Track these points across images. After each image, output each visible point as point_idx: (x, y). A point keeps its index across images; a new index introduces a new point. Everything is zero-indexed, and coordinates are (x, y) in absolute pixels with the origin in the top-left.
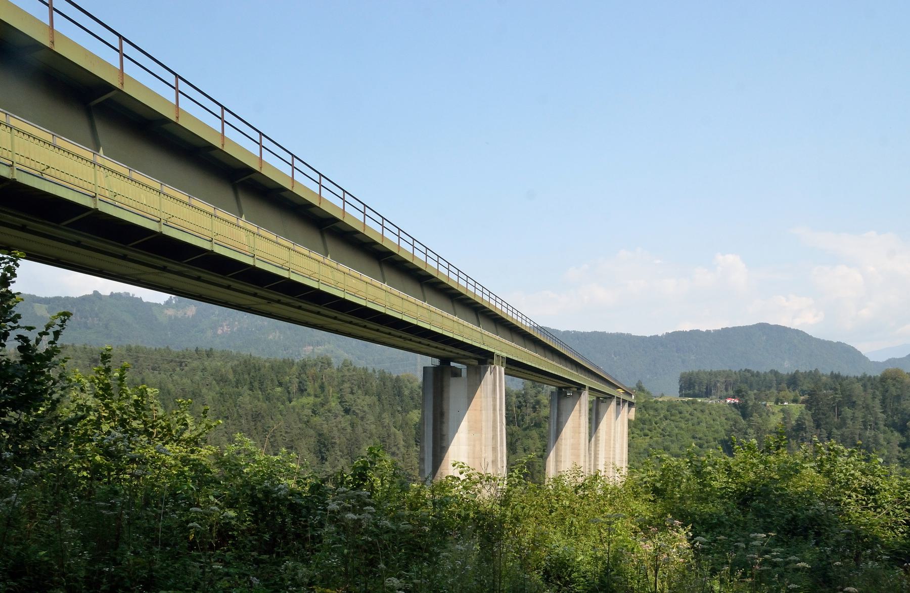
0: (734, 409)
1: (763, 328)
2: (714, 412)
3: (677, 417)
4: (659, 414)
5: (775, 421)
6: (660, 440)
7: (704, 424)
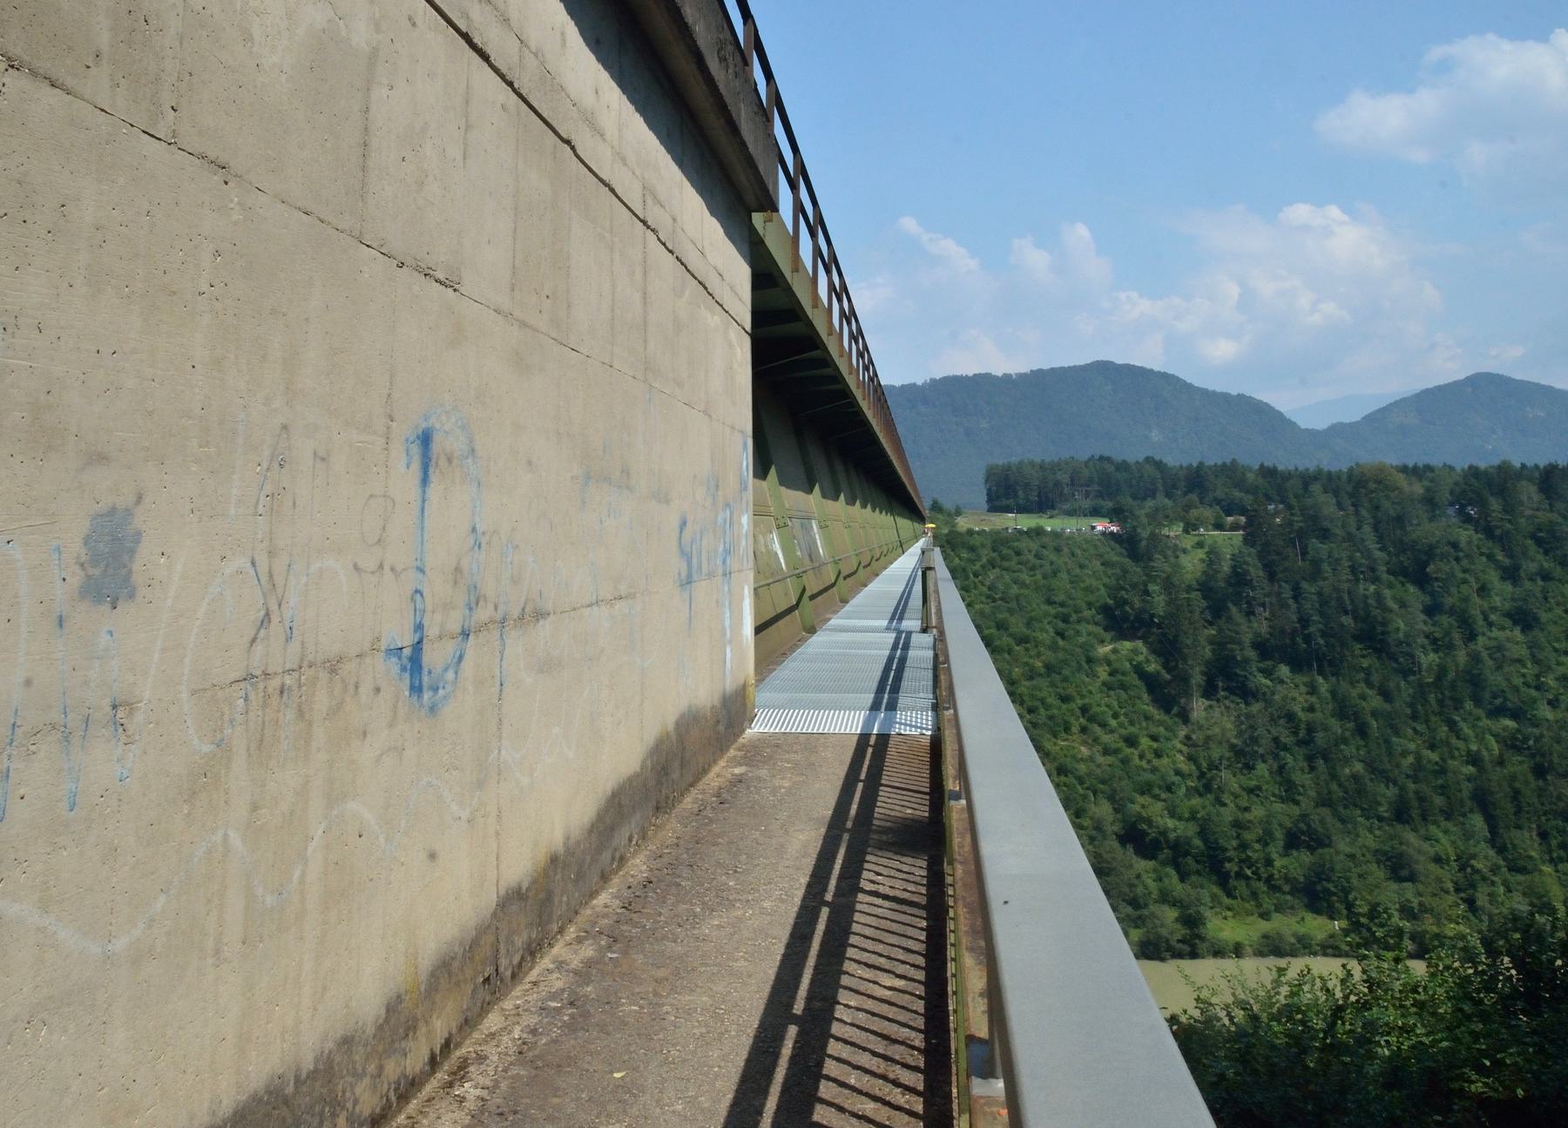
3: (1013, 564)
4: (979, 558)
5: (1192, 564)
6: (987, 609)
7: (1064, 576)
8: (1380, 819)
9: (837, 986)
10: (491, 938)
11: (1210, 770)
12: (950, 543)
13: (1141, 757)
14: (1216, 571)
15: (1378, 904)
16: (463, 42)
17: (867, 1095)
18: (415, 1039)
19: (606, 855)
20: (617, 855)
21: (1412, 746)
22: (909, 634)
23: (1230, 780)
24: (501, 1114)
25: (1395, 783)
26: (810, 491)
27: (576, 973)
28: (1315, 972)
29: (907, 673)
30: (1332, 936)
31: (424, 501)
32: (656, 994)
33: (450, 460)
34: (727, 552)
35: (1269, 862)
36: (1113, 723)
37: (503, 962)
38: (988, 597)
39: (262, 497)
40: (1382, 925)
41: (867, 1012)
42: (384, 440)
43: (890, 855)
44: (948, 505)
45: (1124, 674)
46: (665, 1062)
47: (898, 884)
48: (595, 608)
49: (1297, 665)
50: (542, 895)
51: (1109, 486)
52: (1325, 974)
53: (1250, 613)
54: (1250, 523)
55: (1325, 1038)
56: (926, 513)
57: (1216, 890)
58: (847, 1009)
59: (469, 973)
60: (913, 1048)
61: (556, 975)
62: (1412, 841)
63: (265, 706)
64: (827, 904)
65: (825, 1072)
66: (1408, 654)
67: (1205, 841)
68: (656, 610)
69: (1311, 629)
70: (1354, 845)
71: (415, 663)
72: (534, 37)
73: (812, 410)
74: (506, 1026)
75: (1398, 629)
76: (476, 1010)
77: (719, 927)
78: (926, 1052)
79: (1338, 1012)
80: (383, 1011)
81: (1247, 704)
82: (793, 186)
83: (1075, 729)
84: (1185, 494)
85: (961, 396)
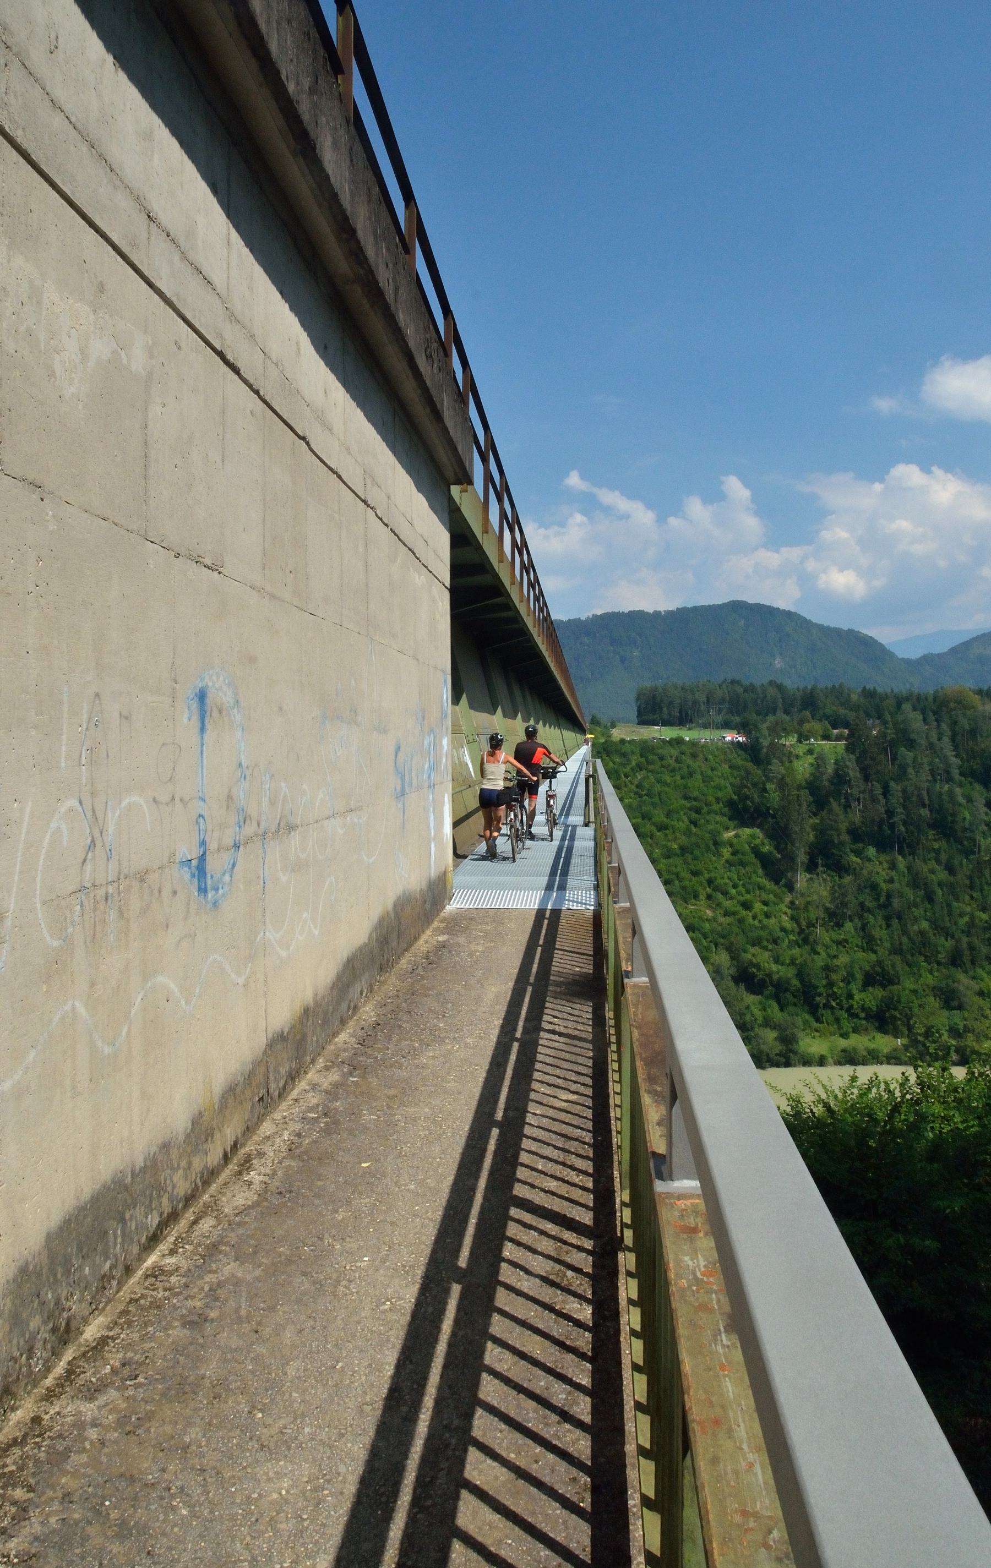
0: (740, 752)
1: (737, 606)
2: (711, 757)
3: (656, 767)
4: (629, 762)
5: (803, 768)
8: (939, 963)
9: (527, 1099)
10: (262, 1069)
11: (808, 927)
12: (602, 750)
13: (754, 918)
14: (822, 774)
15: (933, 1027)
16: (217, 359)
17: (552, 1176)
18: (213, 1142)
19: (344, 1006)
20: (352, 1005)
21: (968, 909)
22: (575, 827)
23: (822, 934)
24: (280, 1193)
25: (953, 937)
26: (493, 712)
27: (327, 1092)
28: (880, 1078)
29: (574, 860)
30: (895, 1050)
31: (202, 745)
32: (389, 1107)
33: (220, 712)
34: (432, 769)
35: (850, 996)
36: (733, 891)
37: (273, 1086)
38: (635, 793)
39: (84, 751)
40: (934, 1042)
41: (550, 1118)
42: (171, 699)
43: (564, 1002)
44: (604, 719)
45: (743, 854)
46: (400, 1155)
47: (570, 1024)
48: (332, 820)
49: (883, 846)
50: (298, 1037)
51: (741, 706)
52: (888, 1078)
53: (847, 807)
54: (852, 734)
55: (885, 1126)
56: (587, 725)
57: (807, 1017)
58: (535, 1115)
59: (248, 1094)
60: (584, 1143)
61: (311, 1094)
62: (964, 982)
63: (95, 909)
64: (517, 1040)
65: (520, 1160)
66: (970, 838)
67: (802, 981)
68: (363, 799)
69: (896, 819)
70: (916, 983)
71: (201, 871)
72: (275, 349)
73: (498, 646)
74: (277, 1132)
75: (964, 819)
76: (255, 1120)
77: (434, 1057)
78: (595, 1146)
79: (896, 1108)
80: (190, 1124)
81: (840, 877)
82: (485, 460)
83: (702, 897)
84: (800, 711)
85: (620, 629)
